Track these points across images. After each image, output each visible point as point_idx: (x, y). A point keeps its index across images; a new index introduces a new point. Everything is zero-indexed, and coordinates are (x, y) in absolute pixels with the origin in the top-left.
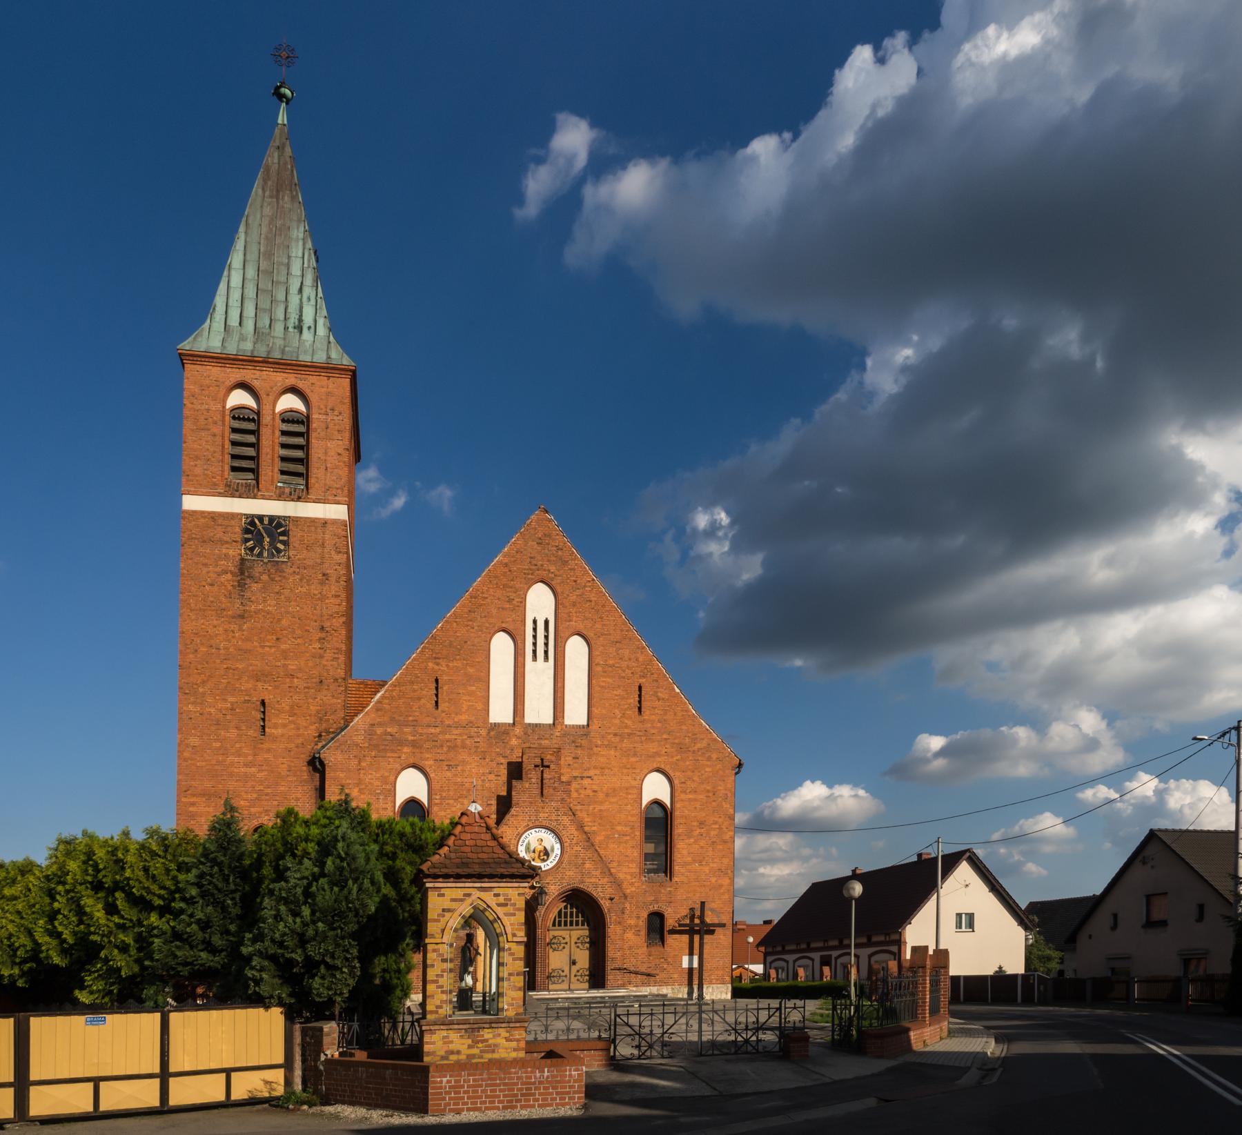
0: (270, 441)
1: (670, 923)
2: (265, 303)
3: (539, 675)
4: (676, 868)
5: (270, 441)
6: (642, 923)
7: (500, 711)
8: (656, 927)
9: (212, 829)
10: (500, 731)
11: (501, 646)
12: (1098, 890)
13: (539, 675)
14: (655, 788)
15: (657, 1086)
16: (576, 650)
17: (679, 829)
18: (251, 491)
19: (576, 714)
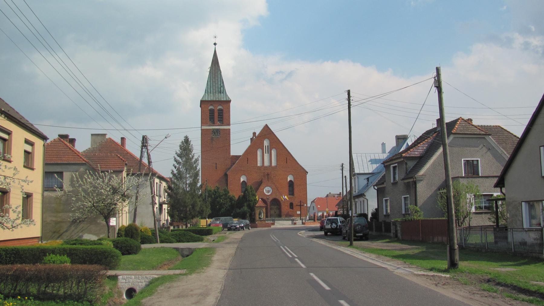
0: (216, 114)
1: (294, 205)
2: (214, 84)
3: (266, 156)
4: (295, 194)
5: (216, 114)
6: (289, 205)
7: (259, 164)
8: (291, 206)
9: (181, 148)
10: (260, 168)
11: (259, 153)
12: (444, 178)
13: (266, 156)
14: (290, 178)
15: (435, 161)
16: (274, 152)
17: (295, 187)
18: (214, 123)
19: (274, 164)
